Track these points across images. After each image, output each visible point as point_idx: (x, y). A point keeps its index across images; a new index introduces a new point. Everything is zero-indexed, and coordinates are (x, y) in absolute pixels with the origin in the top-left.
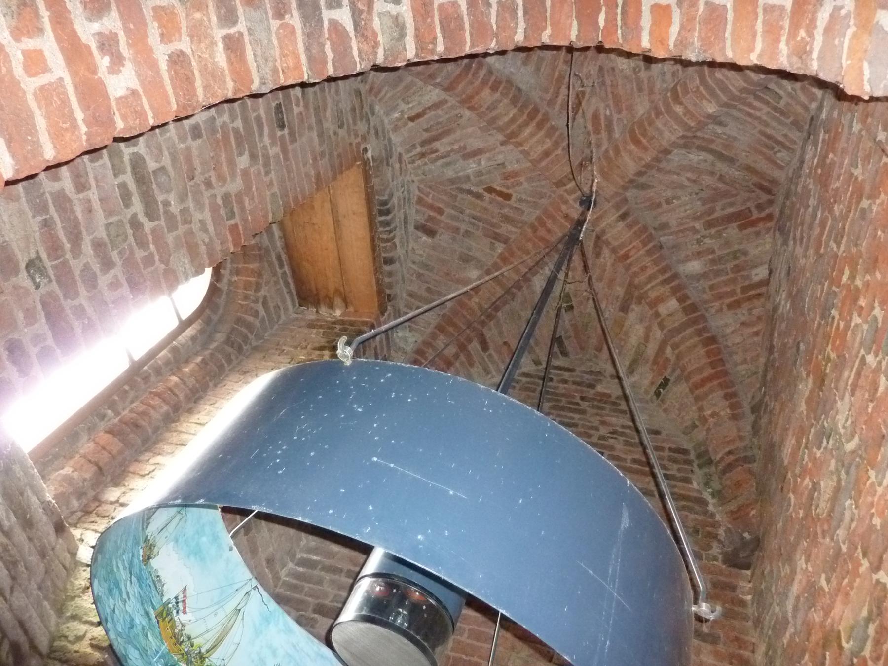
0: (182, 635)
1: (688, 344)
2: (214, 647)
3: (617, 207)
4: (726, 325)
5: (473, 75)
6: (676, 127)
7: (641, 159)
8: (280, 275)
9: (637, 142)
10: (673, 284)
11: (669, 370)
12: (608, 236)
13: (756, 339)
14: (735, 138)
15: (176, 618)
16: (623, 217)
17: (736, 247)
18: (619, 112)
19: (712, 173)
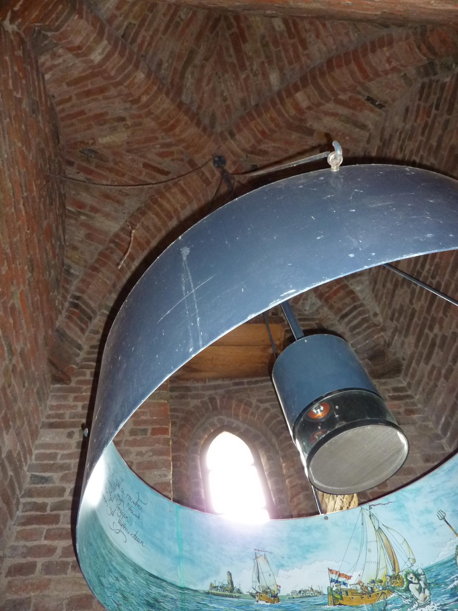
0: (367, 587)
1: (332, 84)
2: (394, 563)
3: (225, 139)
4: (319, 50)
5: (123, 241)
6: (159, 99)
7: (186, 123)
8: (248, 386)
9: (173, 127)
10: (284, 96)
11: (360, 97)
12: (247, 147)
13: (328, 26)
14: (172, 52)
15: (349, 587)
16: (232, 135)
17: (259, 45)
18: (157, 138)
19: (203, 67)
